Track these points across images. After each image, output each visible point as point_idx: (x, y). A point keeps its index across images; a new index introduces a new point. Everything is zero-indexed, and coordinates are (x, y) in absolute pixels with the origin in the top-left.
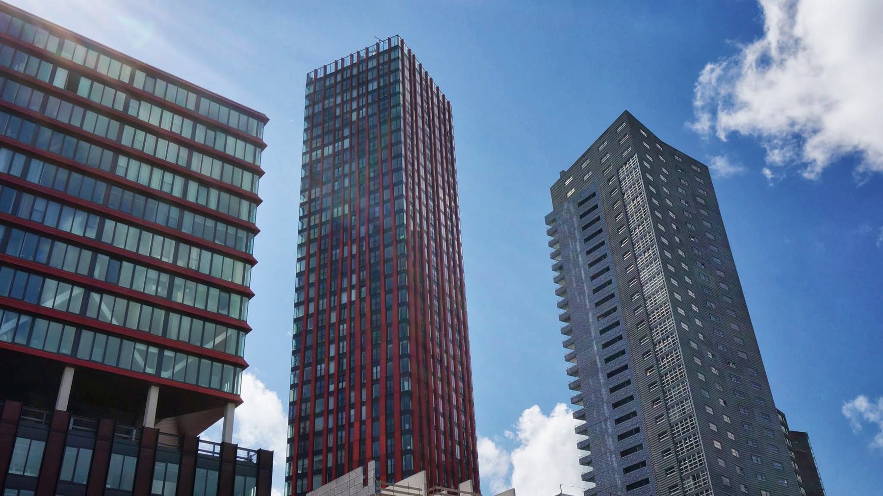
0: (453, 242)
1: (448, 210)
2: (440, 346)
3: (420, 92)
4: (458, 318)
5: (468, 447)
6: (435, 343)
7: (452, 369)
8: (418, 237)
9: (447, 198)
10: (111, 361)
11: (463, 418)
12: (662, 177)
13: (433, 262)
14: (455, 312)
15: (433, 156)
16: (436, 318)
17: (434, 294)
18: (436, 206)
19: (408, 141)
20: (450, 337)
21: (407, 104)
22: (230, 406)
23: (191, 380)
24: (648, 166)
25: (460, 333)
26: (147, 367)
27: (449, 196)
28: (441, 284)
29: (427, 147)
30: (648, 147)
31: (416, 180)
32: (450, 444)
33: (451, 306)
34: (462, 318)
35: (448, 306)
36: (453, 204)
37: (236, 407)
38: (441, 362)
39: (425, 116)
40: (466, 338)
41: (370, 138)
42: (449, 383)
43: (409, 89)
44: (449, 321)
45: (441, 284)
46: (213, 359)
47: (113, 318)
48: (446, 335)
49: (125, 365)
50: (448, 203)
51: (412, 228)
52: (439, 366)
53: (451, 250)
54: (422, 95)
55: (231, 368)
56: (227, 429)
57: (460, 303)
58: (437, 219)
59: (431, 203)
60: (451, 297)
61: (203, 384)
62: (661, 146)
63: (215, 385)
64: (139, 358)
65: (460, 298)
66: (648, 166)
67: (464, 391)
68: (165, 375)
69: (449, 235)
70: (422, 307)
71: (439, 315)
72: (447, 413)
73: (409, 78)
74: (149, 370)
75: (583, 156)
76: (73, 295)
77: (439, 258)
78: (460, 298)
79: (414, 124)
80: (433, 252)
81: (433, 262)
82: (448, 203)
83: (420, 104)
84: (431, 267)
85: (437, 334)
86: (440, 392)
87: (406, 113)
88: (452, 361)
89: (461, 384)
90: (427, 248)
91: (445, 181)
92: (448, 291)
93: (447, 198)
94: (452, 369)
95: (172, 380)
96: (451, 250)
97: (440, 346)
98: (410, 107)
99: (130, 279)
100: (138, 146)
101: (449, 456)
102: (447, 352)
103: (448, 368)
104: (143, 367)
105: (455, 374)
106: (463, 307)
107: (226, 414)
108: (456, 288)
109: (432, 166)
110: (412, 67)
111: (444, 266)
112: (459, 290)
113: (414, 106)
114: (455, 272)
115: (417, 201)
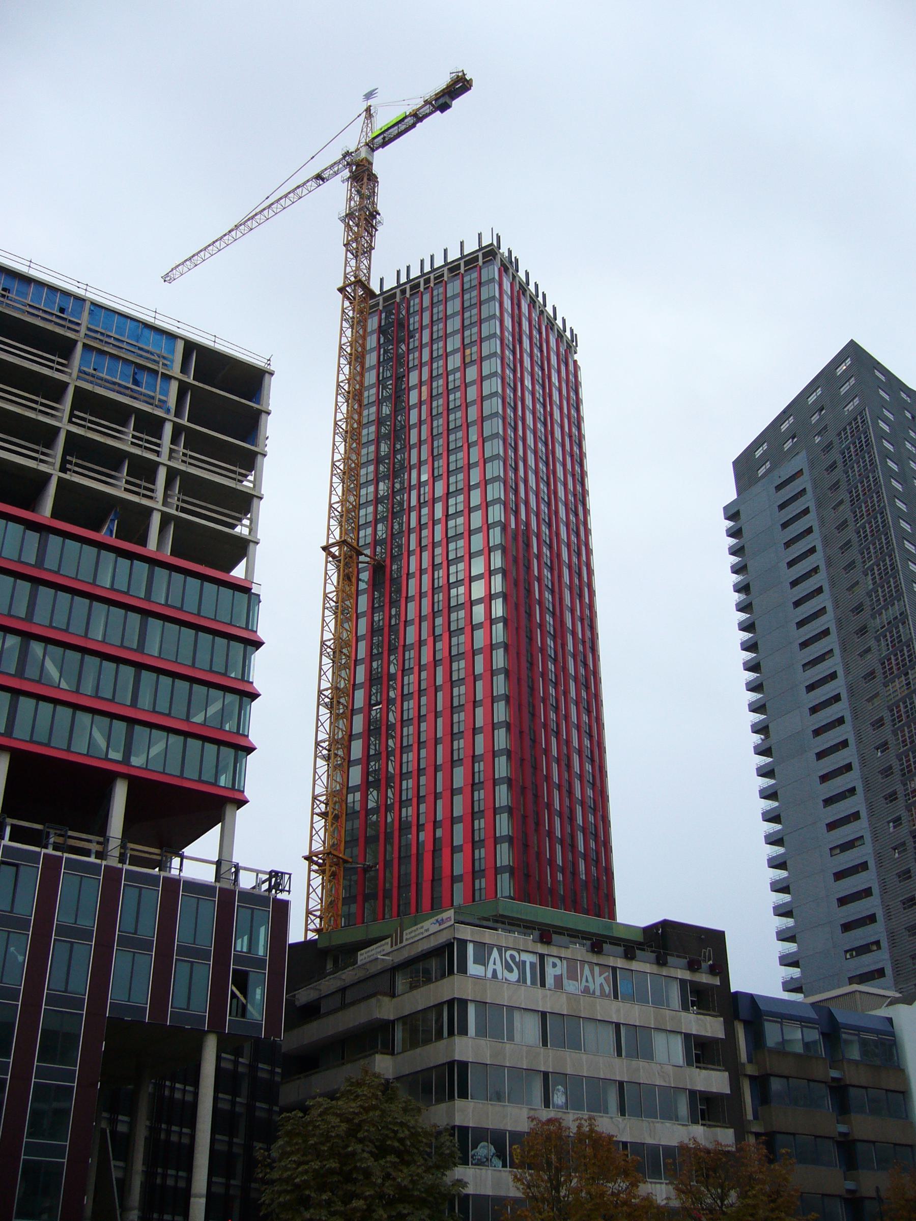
0: (581, 589)
1: (571, 498)
2: (557, 709)
3: (528, 332)
4: (586, 665)
5: (597, 861)
6: (549, 730)
7: (575, 743)
8: (523, 541)
9: (568, 459)
10: (59, 741)
11: (591, 818)
12: (908, 446)
13: (546, 580)
14: (580, 657)
15: (546, 377)
16: (551, 666)
17: (548, 629)
18: (553, 513)
19: (508, 391)
20: (573, 694)
21: (506, 334)
22: (229, 809)
23: (173, 769)
24: (886, 428)
25: (587, 688)
26: (110, 750)
27: (573, 475)
28: (558, 613)
29: (535, 326)
30: (887, 397)
31: (521, 452)
32: (565, 751)
33: (576, 695)
34: (591, 666)
35: (570, 647)
36: (579, 488)
37: (238, 809)
38: (558, 734)
39: (536, 351)
40: (596, 673)
41: (453, 679)
42: (569, 766)
43: (510, 310)
44: (572, 671)
45: (558, 613)
46: (205, 739)
47: (62, 679)
48: (566, 693)
49: (80, 746)
50: (569, 467)
51: (513, 526)
52: (554, 741)
53: (575, 560)
54: (531, 337)
55: (231, 752)
56: (226, 842)
57: (588, 644)
58: (555, 555)
59: (542, 466)
60: (574, 634)
61: (191, 773)
62: (908, 396)
63: (208, 776)
64: (100, 740)
65: (588, 634)
66: (886, 428)
67: (594, 776)
68: (137, 761)
69: (571, 516)
70: (530, 675)
71: (555, 661)
72: (565, 785)
73: (509, 293)
74: (113, 755)
75: (784, 412)
76: (5, 647)
77: (557, 596)
78: (588, 634)
79: (518, 365)
80: (546, 564)
81: (546, 580)
82: (569, 467)
83: (527, 315)
84: (544, 587)
85: (552, 691)
86: (556, 779)
87: (506, 347)
88: (575, 733)
89: (590, 792)
90: (537, 559)
91: (567, 453)
92: (569, 624)
93: (568, 459)
94: (575, 743)
95: (146, 769)
96: (575, 560)
97: (557, 709)
98: (511, 339)
99: (17, 896)
100: (68, 570)
101: (569, 875)
102: (567, 717)
103: (568, 742)
104: (105, 750)
105: (580, 752)
106: (594, 649)
107: (224, 819)
108: (582, 620)
109: (549, 489)
110: (517, 329)
111: (563, 585)
112: (586, 622)
113: (517, 337)
114: (581, 596)
115: (520, 424)
